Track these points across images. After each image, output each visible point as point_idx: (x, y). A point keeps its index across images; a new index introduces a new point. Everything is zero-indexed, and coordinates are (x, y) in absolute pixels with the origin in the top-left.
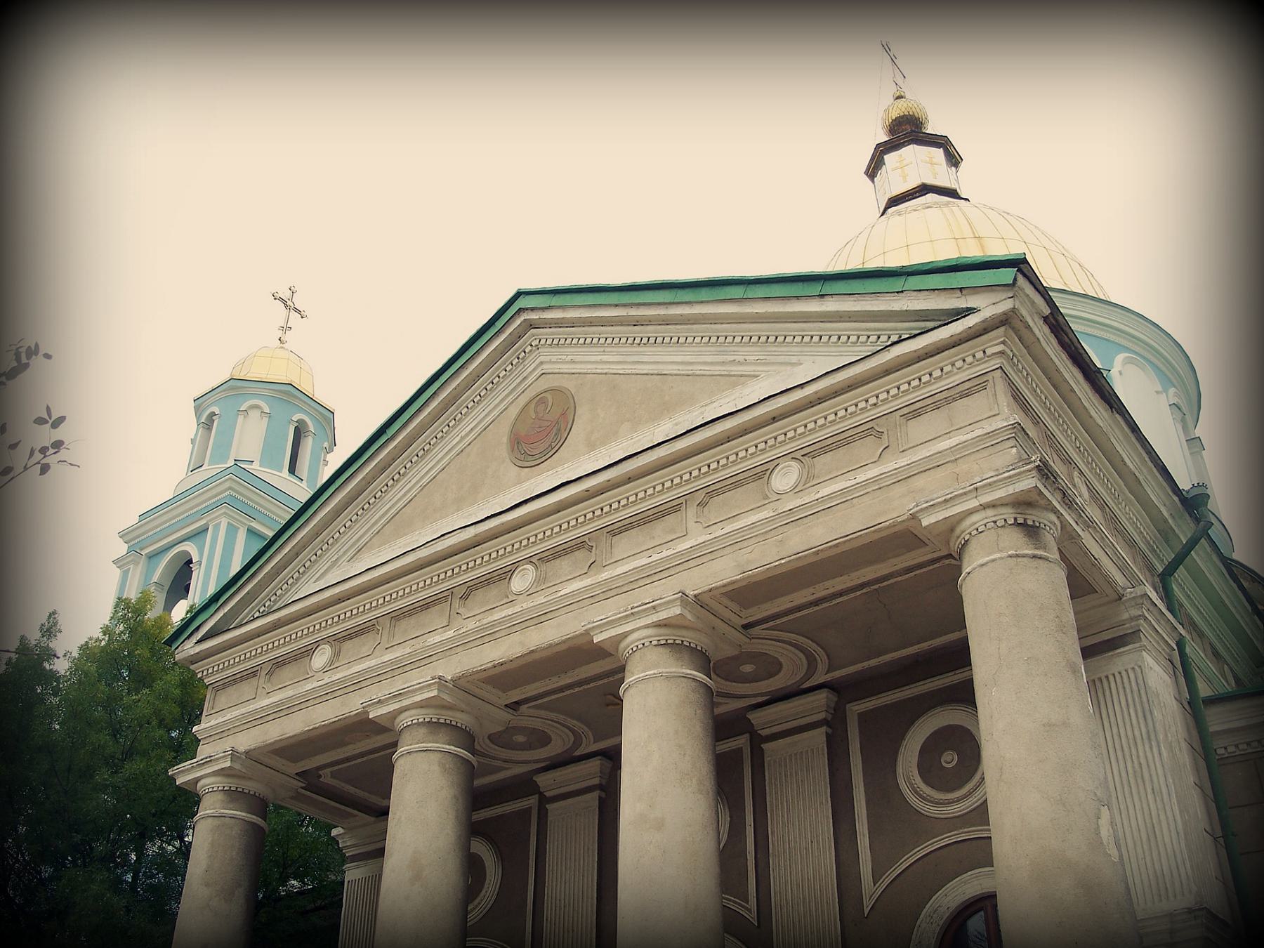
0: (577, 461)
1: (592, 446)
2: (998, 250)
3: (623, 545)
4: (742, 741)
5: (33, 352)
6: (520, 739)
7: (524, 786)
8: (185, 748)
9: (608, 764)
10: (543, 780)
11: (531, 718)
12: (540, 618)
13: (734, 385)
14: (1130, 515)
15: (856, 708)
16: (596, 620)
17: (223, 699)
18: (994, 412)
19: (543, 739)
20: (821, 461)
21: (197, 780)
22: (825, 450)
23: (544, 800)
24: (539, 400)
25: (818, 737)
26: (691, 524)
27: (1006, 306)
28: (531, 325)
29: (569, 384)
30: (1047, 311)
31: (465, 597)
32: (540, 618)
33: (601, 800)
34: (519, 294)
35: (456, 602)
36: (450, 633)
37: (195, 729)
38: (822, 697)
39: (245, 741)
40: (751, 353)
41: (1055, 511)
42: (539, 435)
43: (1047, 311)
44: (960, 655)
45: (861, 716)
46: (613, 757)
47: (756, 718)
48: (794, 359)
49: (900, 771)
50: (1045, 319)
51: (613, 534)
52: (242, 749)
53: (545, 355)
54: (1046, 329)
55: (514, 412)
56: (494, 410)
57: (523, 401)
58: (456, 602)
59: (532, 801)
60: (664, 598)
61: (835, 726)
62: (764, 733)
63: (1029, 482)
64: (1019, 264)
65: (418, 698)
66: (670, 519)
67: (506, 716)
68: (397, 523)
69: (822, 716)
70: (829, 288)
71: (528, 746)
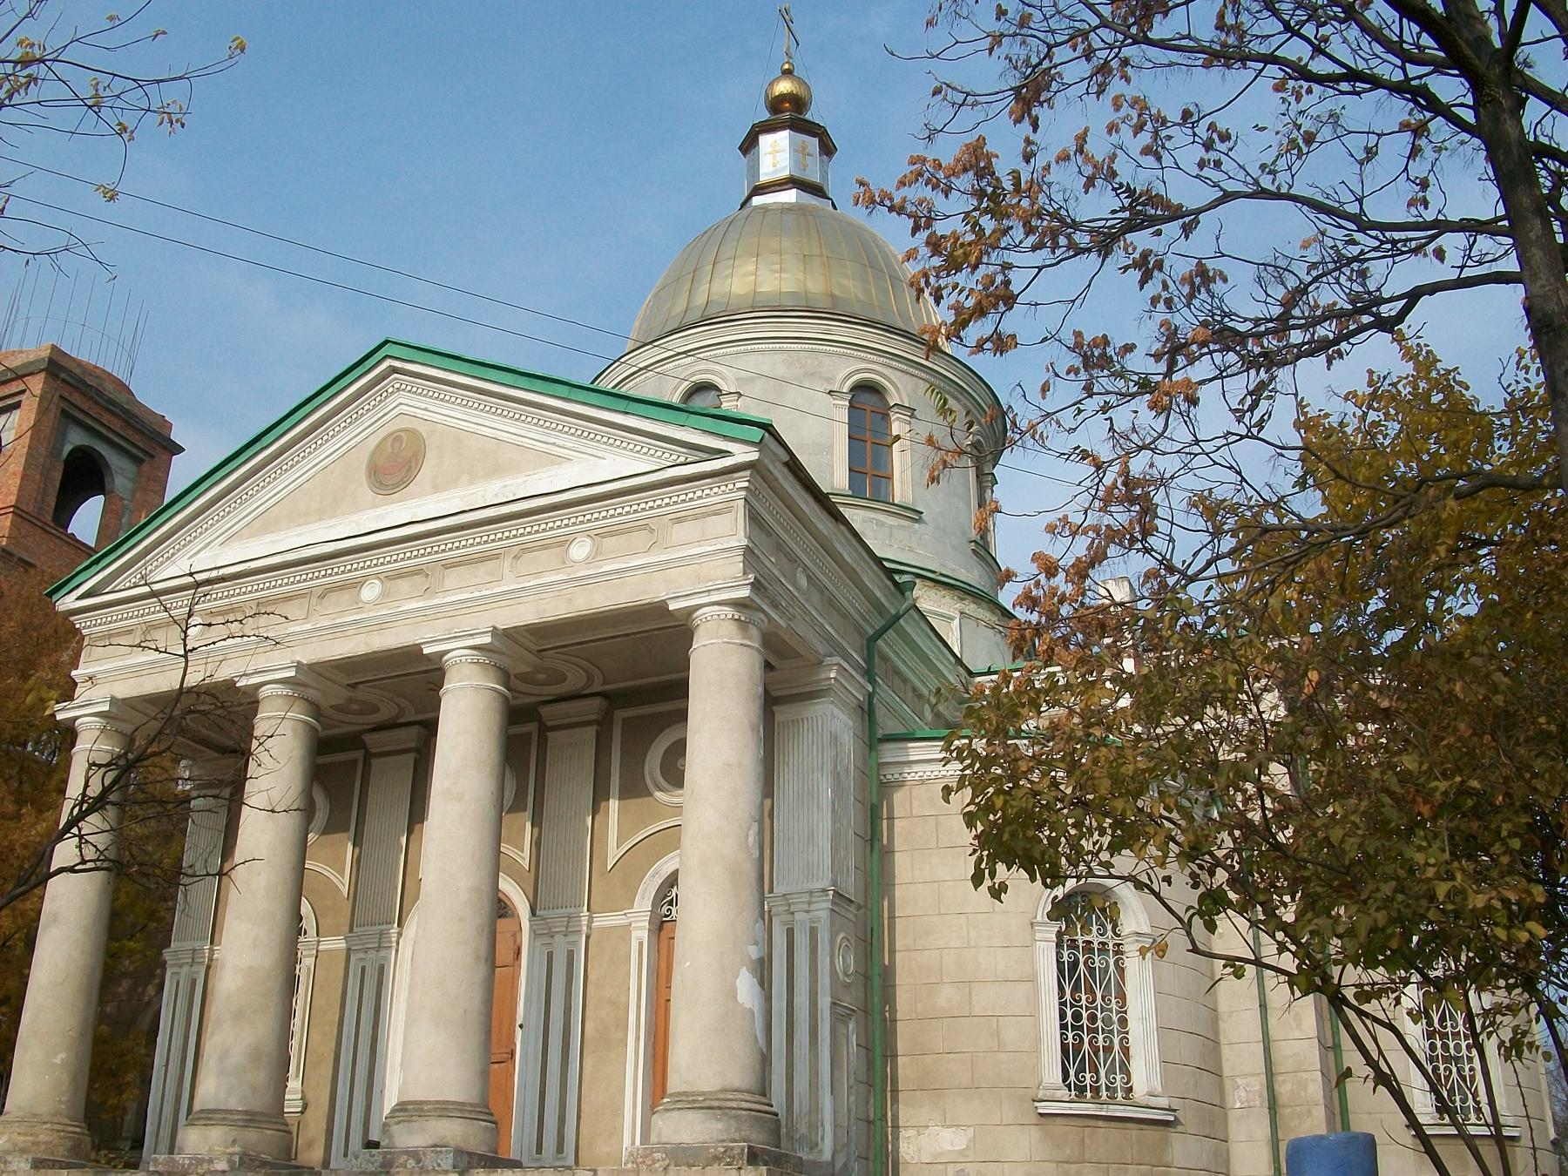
0: (420, 505)
1: (436, 489)
2: (756, 414)
3: (453, 578)
4: (532, 727)
5: (461, 919)
6: (356, 707)
7: (353, 741)
8: (68, 691)
9: (605, 703)
10: (370, 739)
11: (363, 694)
12: (382, 625)
13: (553, 463)
14: (847, 597)
15: (621, 715)
16: (428, 636)
17: (98, 652)
18: (732, 531)
19: (375, 709)
20: (609, 542)
21: (77, 718)
22: (612, 534)
23: (368, 756)
24: (395, 438)
25: (590, 732)
26: (506, 572)
27: (754, 456)
28: (395, 370)
29: (422, 429)
30: (786, 458)
31: (322, 597)
32: (382, 625)
33: (416, 761)
34: (386, 342)
35: (314, 600)
36: (309, 626)
37: (73, 673)
38: (597, 701)
39: (125, 690)
40: (569, 442)
41: (763, 611)
42: (394, 468)
43: (786, 458)
44: (679, 689)
45: (624, 720)
46: (429, 728)
47: (545, 711)
48: (600, 454)
49: (646, 767)
50: (786, 464)
51: (446, 567)
52: (119, 696)
53: (402, 398)
54: (785, 470)
55: (373, 442)
56: (351, 439)
57: (382, 434)
58: (314, 600)
59: (359, 755)
60: (482, 624)
61: (603, 726)
62: (549, 724)
63: (745, 592)
64: (767, 427)
65: (278, 676)
66: (491, 565)
67: (346, 693)
68: (266, 523)
69: (594, 717)
70: (633, 407)
71: (360, 713)
